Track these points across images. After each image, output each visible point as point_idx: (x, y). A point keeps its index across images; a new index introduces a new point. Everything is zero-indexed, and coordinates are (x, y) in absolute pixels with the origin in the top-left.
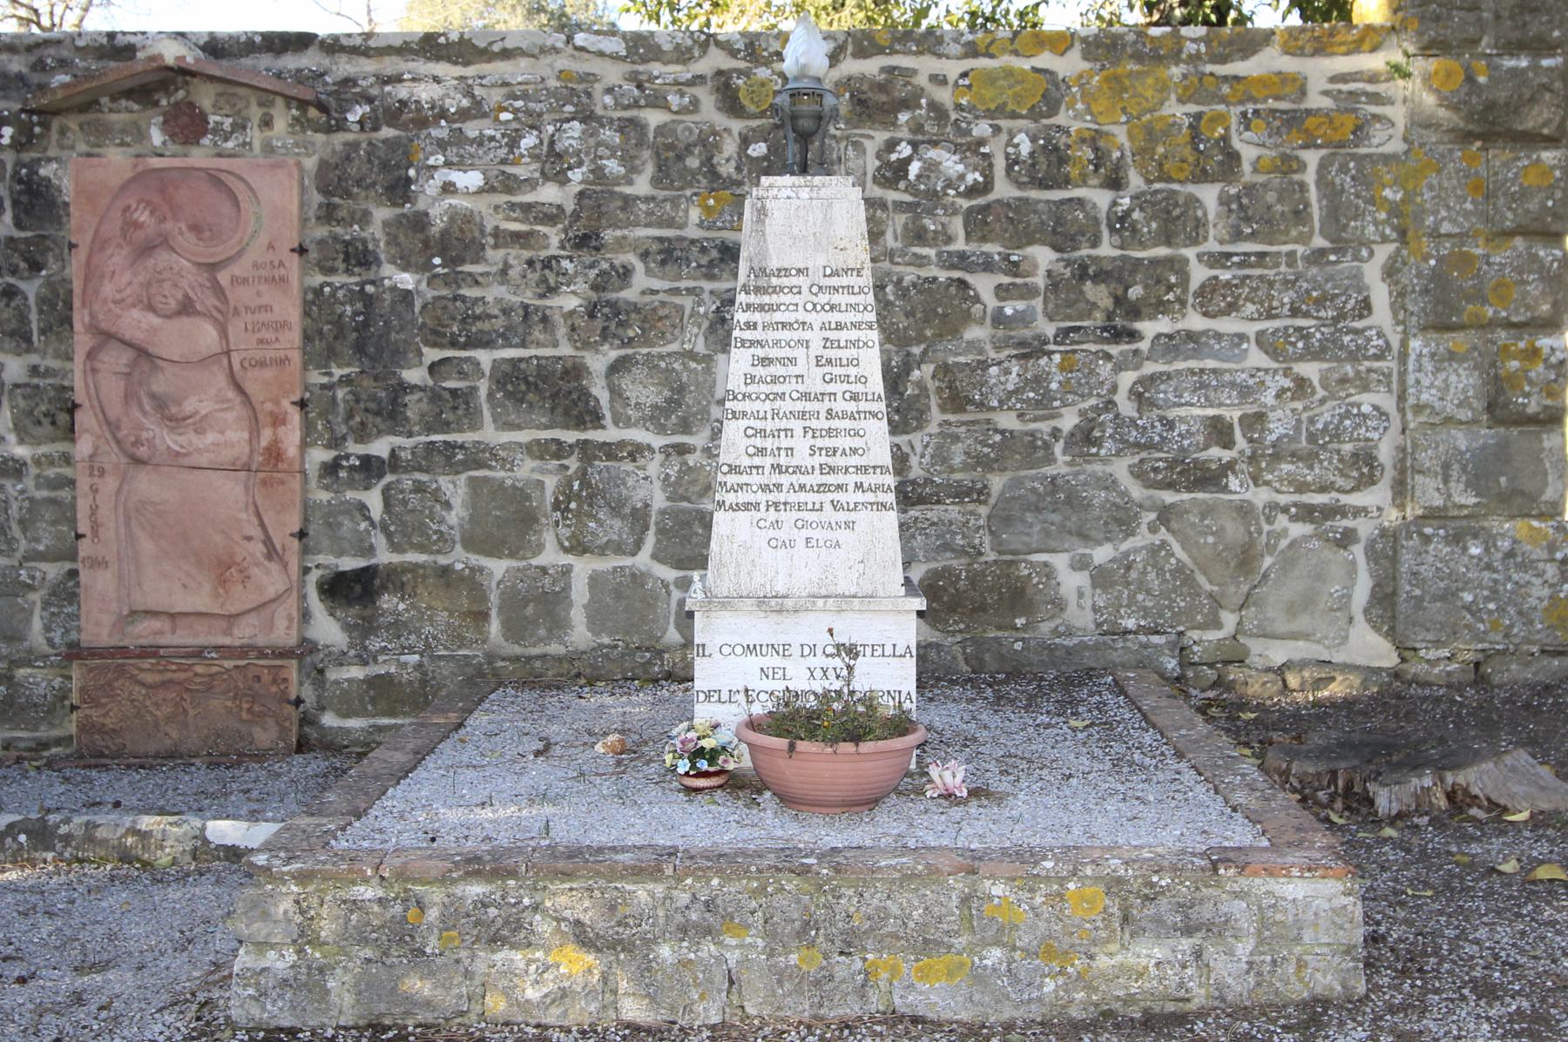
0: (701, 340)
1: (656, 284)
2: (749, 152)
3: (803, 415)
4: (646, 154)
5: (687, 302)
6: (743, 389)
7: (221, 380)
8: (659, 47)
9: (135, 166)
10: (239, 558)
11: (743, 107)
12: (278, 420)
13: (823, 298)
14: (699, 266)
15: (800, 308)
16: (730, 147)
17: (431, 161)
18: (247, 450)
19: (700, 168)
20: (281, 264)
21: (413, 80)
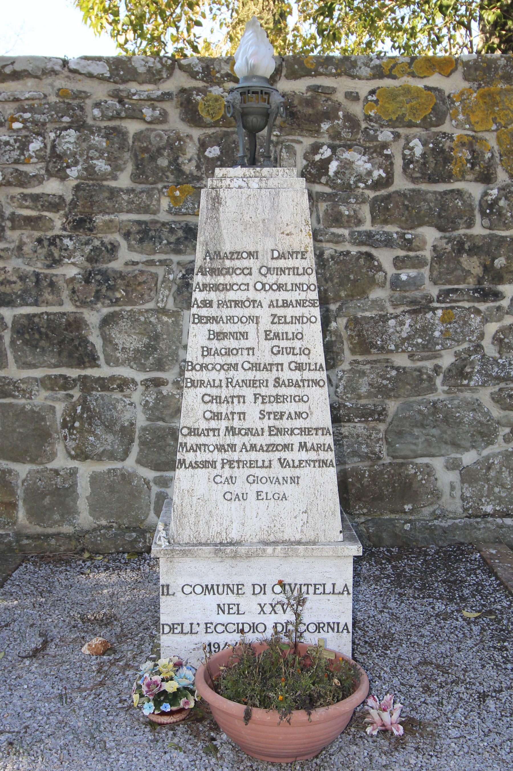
0: (171, 300)
1: (136, 257)
2: (206, 153)
3: (253, 383)
4: (127, 155)
5: (161, 271)
6: (201, 360)
8: (135, 69)
11: (201, 118)
13: (272, 279)
14: (169, 243)
15: (251, 288)
19: (168, 167)
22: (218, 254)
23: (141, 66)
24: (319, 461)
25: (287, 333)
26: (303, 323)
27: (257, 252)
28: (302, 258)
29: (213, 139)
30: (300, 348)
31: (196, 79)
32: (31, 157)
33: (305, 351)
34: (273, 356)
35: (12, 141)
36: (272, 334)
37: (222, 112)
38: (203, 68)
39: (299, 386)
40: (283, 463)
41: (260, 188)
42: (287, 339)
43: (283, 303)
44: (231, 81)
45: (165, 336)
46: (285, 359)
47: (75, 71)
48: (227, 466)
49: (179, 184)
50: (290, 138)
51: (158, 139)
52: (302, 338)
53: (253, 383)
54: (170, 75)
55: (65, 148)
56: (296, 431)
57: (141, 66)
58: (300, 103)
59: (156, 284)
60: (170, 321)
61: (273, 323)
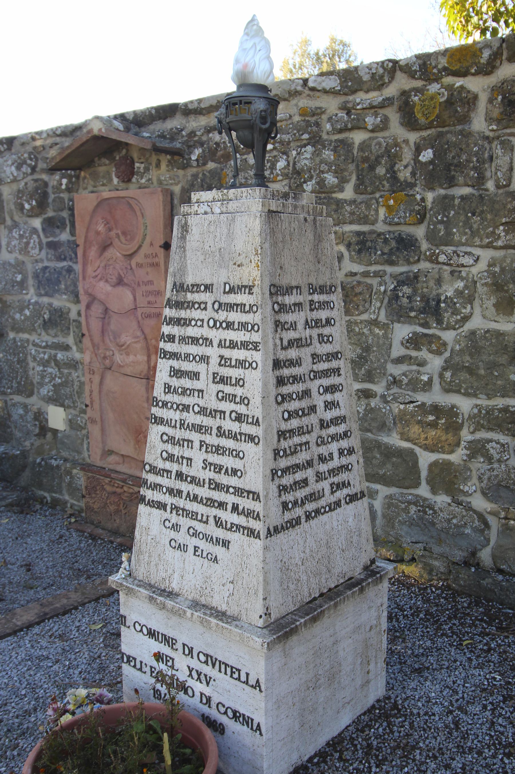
0: (383, 312)
1: (357, 268)
2: (420, 158)
3: (199, 428)
4: (352, 167)
5: (374, 282)
6: (163, 397)
7: (134, 324)
8: (361, 78)
9: (98, 198)
11: (416, 120)
13: (222, 315)
14: (383, 254)
15: (205, 324)
16: (407, 156)
18: (146, 367)
20: (156, 255)
22: (182, 286)
23: (366, 73)
24: (248, 528)
25: (231, 378)
26: (245, 368)
27: (212, 285)
28: (249, 293)
30: (241, 397)
31: (416, 79)
32: (278, 175)
33: (244, 401)
34: (218, 402)
37: (437, 111)
38: (420, 66)
40: (218, 523)
41: (222, 213)
42: (231, 385)
43: (230, 344)
44: (448, 75)
45: (375, 349)
46: (227, 406)
47: (313, 89)
48: (174, 512)
49: (394, 192)
50: (508, 131)
51: (377, 147)
52: (243, 386)
53: (199, 428)
55: (303, 164)
56: (231, 490)
59: (371, 296)
60: (381, 334)
61: (220, 365)
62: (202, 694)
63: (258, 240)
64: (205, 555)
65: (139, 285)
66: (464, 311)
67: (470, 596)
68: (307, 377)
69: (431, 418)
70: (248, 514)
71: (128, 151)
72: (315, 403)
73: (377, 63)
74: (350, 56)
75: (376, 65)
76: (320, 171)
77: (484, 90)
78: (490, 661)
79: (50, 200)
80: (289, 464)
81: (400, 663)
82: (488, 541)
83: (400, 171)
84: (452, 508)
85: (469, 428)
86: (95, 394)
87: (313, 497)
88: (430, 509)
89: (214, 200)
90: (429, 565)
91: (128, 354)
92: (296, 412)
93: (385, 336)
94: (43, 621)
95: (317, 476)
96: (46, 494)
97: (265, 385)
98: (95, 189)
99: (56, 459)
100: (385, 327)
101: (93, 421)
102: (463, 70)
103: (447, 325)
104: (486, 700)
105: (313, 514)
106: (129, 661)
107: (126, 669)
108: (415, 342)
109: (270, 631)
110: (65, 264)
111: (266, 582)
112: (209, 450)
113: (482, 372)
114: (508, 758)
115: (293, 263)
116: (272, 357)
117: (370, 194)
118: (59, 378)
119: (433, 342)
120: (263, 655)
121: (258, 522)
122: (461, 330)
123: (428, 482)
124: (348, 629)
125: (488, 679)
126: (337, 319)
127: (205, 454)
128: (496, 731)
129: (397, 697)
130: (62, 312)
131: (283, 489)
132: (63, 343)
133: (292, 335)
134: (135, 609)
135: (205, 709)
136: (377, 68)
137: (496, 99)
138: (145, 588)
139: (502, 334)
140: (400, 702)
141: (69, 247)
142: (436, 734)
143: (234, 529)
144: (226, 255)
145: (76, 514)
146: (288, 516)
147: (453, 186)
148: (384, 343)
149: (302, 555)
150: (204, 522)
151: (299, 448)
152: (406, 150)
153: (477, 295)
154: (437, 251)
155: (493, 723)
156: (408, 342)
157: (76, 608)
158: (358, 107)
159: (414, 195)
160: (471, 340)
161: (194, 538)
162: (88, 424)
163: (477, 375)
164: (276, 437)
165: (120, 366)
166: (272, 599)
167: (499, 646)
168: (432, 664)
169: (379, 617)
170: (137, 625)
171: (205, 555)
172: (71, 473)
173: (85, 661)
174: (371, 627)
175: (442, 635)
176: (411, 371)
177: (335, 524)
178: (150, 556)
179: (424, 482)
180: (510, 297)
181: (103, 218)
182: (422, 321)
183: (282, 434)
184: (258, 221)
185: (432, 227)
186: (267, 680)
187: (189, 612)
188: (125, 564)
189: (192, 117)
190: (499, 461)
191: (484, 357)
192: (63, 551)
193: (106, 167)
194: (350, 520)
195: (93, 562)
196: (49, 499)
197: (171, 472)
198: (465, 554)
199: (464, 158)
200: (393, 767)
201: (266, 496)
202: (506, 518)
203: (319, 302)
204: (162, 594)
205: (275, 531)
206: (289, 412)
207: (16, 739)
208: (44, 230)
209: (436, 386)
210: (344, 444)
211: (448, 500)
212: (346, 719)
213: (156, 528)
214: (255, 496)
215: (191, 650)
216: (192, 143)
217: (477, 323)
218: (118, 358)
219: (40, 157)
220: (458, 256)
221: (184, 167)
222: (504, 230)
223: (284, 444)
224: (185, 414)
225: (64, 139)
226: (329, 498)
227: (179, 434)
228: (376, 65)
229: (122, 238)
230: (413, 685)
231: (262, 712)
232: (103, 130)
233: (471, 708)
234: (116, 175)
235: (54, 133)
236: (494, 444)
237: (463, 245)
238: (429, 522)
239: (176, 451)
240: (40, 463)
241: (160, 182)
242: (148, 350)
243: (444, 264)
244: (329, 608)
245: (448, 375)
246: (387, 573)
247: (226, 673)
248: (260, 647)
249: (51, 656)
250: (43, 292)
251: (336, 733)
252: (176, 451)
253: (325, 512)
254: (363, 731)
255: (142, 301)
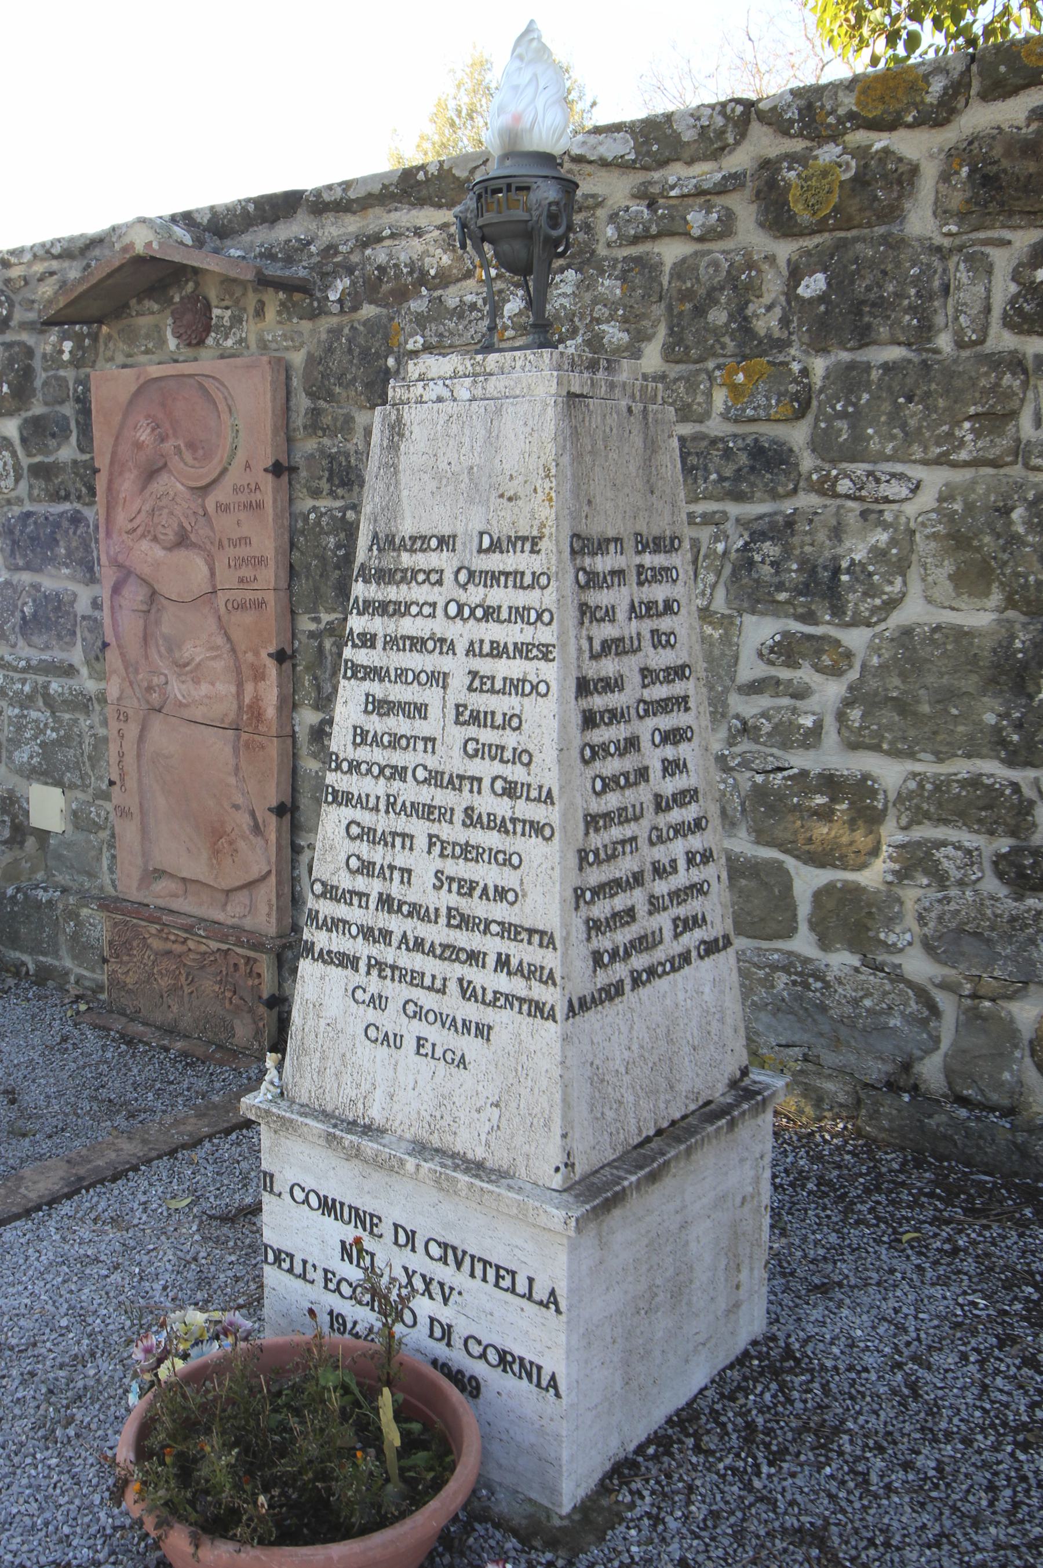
0: (720, 594)
2: (800, 291)
3: (428, 812)
4: (658, 310)
6: (350, 753)
10: (228, 829)
11: (792, 217)
12: (259, 676)
13: (475, 595)
14: (722, 479)
15: (439, 612)
17: (410, 346)
18: (235, 706)
19: (727, 325)
20: (257, 487)
21: (393, 236)
22: (390, 539)
23: (689, 127)
24: (531, 1001)
25: (493, 713)
26: (523, 695)
27: (455, 537)
28: (532, 551)
29: (814, 259)
31: (792, 137)
32: (505, 328)
33: (522, 757)
34: (466, 760)
35: (480, 302)
36: (467, 713)
37: (835, 199)
38: (800, 110)
39: (507, 832)
40: (467, 992)
41: (473, 399)
42: (493, 727)
48: (375, 972)
49: (745, 358)
50: (982, 235)
51: (711, 270)
52: (518, 728)
53: (428, 812)
54: (742, 135)
55: (557, 305)
56: (495, 928)
57: (689, 127)
58: (1008, 153)
60: (716, 635)
61: (470, 689)
62: (432, 1320)
63: (551, 449)
64: (439, 1053)
65: (221, 545)
66: (888, 589)
67: (903, 1149)
68: (633, 711)
69: (820, 800)
70: (530, 973)
71: (197, 284)
72: (646, 763)
73: (712, 107)
74: (569, 92)
75: (709, 111)
76: (593, 319)
77: (931, 156)
78: (959, 1272)
79: (38, 383)
80: (604, 878)
81: (784, 1275)
82: (937, 1040)
83: (757, 316)
84: (863, 977)
85: (898, 818)
86: (130, 760)
87: (645, 943)
88: (818, 978)
89: (455, 375)
90: (816, 1089)
91: (197, 681)
92: (615, 779)
93: (726, 640)
94: (77, 1192)
95: (651, 904)
96: (25, 958)
97: (563, 726)
98: (130, 361)
99: (45, 889)
100: (726, 622)
101: (124, 812)
102: (888, 118)
103: (853, 617)
104: (964, 1344)
105: (644, 976)
106: (278, 1260)
107: (272, 1275)
108: (786, 651)
109: (576, 1196)
110: (66, 506)
111: (566, 1102)
112: (449, 851)
113: (925, 708)
114: (1025, 1451)
115: (610, 494)
116: (574, 674)
117: (696, 362)
118: (53, 730)
119: (825, 651)
120: (565, 1241)
121: (551, 988)
122: (882, 626)
123: (813, 926)
124: (705, 1200)
125: (961, 1306)
126: (683, 602)
127: (438, 860)
128: (993, 1402)
129: (789, 1336)
130: (60, 601)
131: (594, 926)
132: (61, 661)
133: (607, 631)
134: (294, 1159)
135: (440, 1350)
136: (711, 116)
137: (957, 173)
138: (316, 1118)
139: (967, 633)
140: (797, 1346)
141: (76, 474)
142: (876, 1407)
143: (502, 1001)
144: (484, 479)
145: (89, 994)
146: (603, 978)
147: (867, 345)
148: (723, 655)
149: (627, 1053)
150: (438, 991)
151: (620, 848)
152: (770, 275)
153: (914, 558)
154: (834, 472)
155: (985, 1387)
156: (772, 651)
157: (135, 1169)
158: (672, 193)
159: (786, 364)
160: (903, 646)
161: (415, 1021)
162: (112, 816)
163: (915, 714)
164: (582, 826)
165: (181, 705)
166: (577, 1136)
167: (974, 1243)
168: (847, 1277)
169: (757, 1180)
170: (297, 1191)
171: (439, 1053)
172: (78, 915)
173: (169, 1267)
174: (744, 1199)
175: (858, 1222)
176: (778, 709)
177: (681, 995)
178: (323, 1058)
179: (803, 927)
180: (984, 561)
181: (148, 417)
182: (800, 610)
183: (592, 822)
184: (550, 412)
185: (823, 425)
186: (570, 1291)
187: (411, 1163)
188: (272, 1074)
189: (329, 217)
190: (961, 883)
191: (930, 680)
192: (73, 1066)
193: (154, 319)
194: (707, 990)
195: (135, 1086)
196: (31, 967)
197: (368, 896)
198: (889, 1068)
199: (891, 289)
200: (801, 1465)
201: (566, 939)
202: (975, 996)
203: (653, 569)
204: (350, 1130)
205: (581, 1006)
206: (603, 779)
207: (67, 1407)
208: (24, 440)
209: (831, 736)
210: (696, 842)
211: (855, 961)
212: (699, 1376)
213: (336, 1004)
214: (546, 939)
215: (411, 1236)
216: (329, 268)
217: (914, 612)
218: (177, 689)
219: (16, 298)
220: (878, 481)
221: (313, 315)
222: (972, 430)
223: (597, 840)
224: (397, 784)
225: (66, 264)
226: (670, 948)
227: (383, 823)
228: (709, 111)
229: (188, 456)
230: (816, 1314)
231: (560, 1353)
232: (155, 245)
233: (935, 1358)
234: (173, 333)
235: (48, 252)
236: (950, 850)
237: (888, 459)
238: (816, 1005)
239: (378, 855)
240: (13, 897)
241: (263, 345)
242: (239, 672)
243: (848, 497)
244: (676, 1157)
245: (855, 714)
246: (774, 1094)
247: (484, 1279)
248: (560, 1227)
249: (103, 1258)
250: (21, 563)
251: (681, 1402)
252: (378, 855)
253: (665, 973)
254: (733, 1399)
255: (226, 578)
